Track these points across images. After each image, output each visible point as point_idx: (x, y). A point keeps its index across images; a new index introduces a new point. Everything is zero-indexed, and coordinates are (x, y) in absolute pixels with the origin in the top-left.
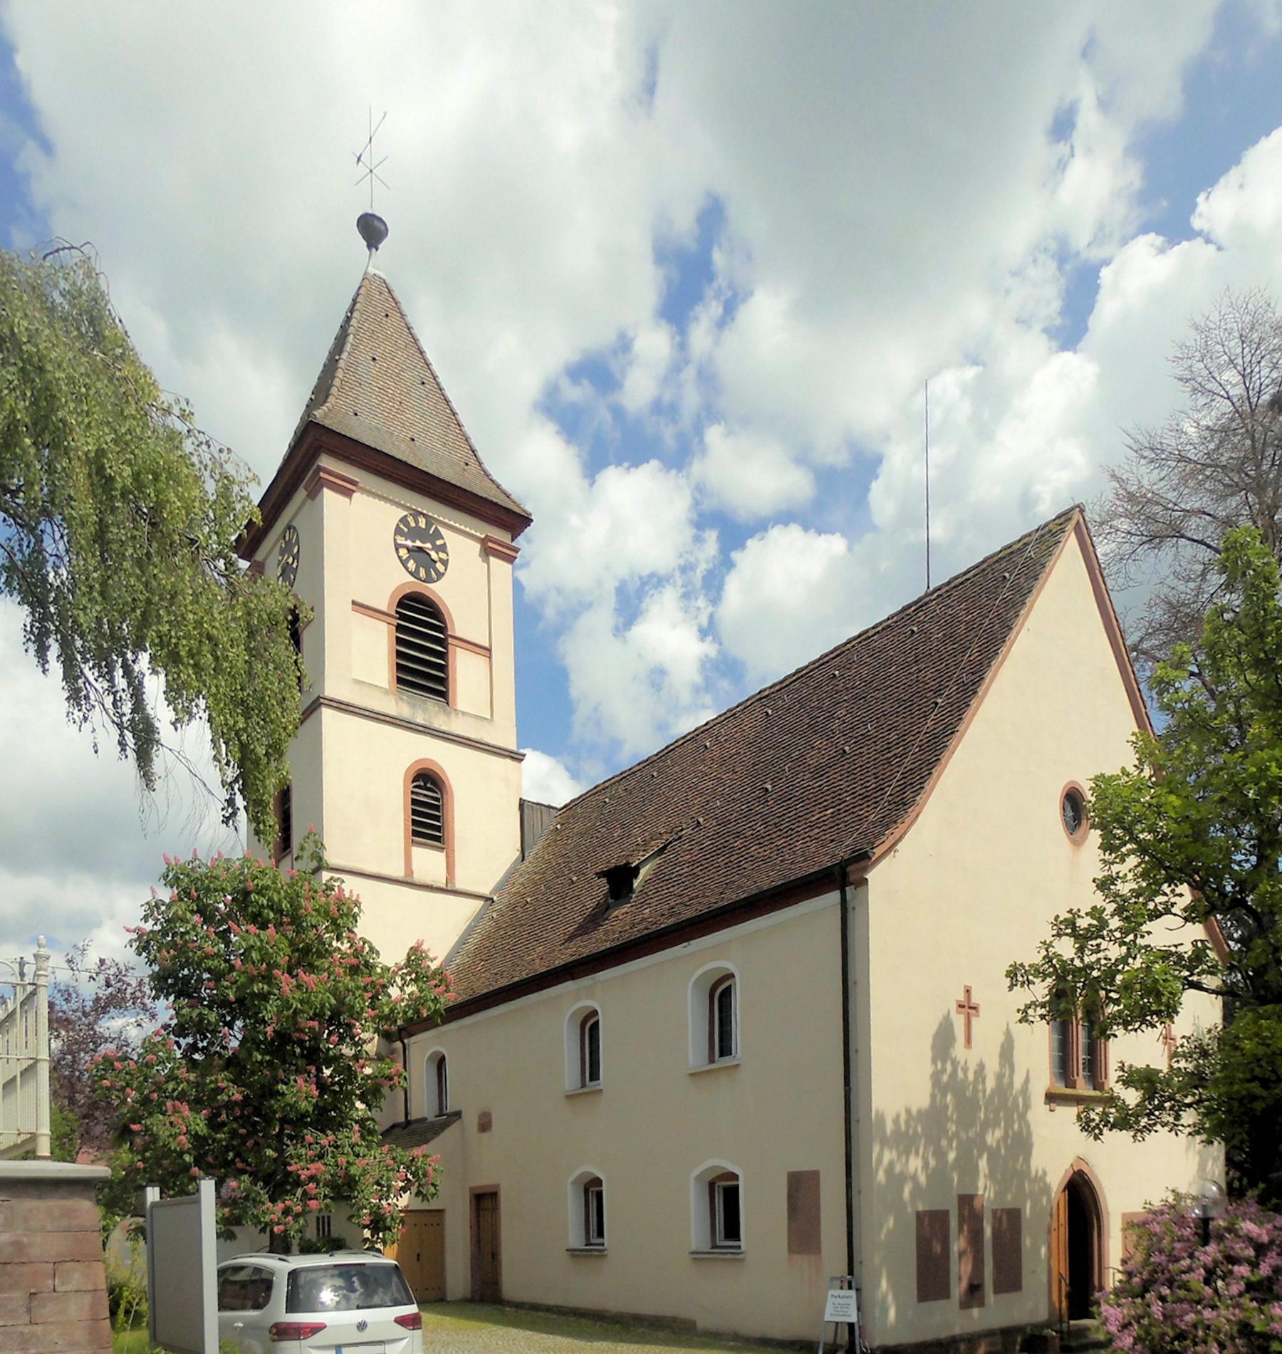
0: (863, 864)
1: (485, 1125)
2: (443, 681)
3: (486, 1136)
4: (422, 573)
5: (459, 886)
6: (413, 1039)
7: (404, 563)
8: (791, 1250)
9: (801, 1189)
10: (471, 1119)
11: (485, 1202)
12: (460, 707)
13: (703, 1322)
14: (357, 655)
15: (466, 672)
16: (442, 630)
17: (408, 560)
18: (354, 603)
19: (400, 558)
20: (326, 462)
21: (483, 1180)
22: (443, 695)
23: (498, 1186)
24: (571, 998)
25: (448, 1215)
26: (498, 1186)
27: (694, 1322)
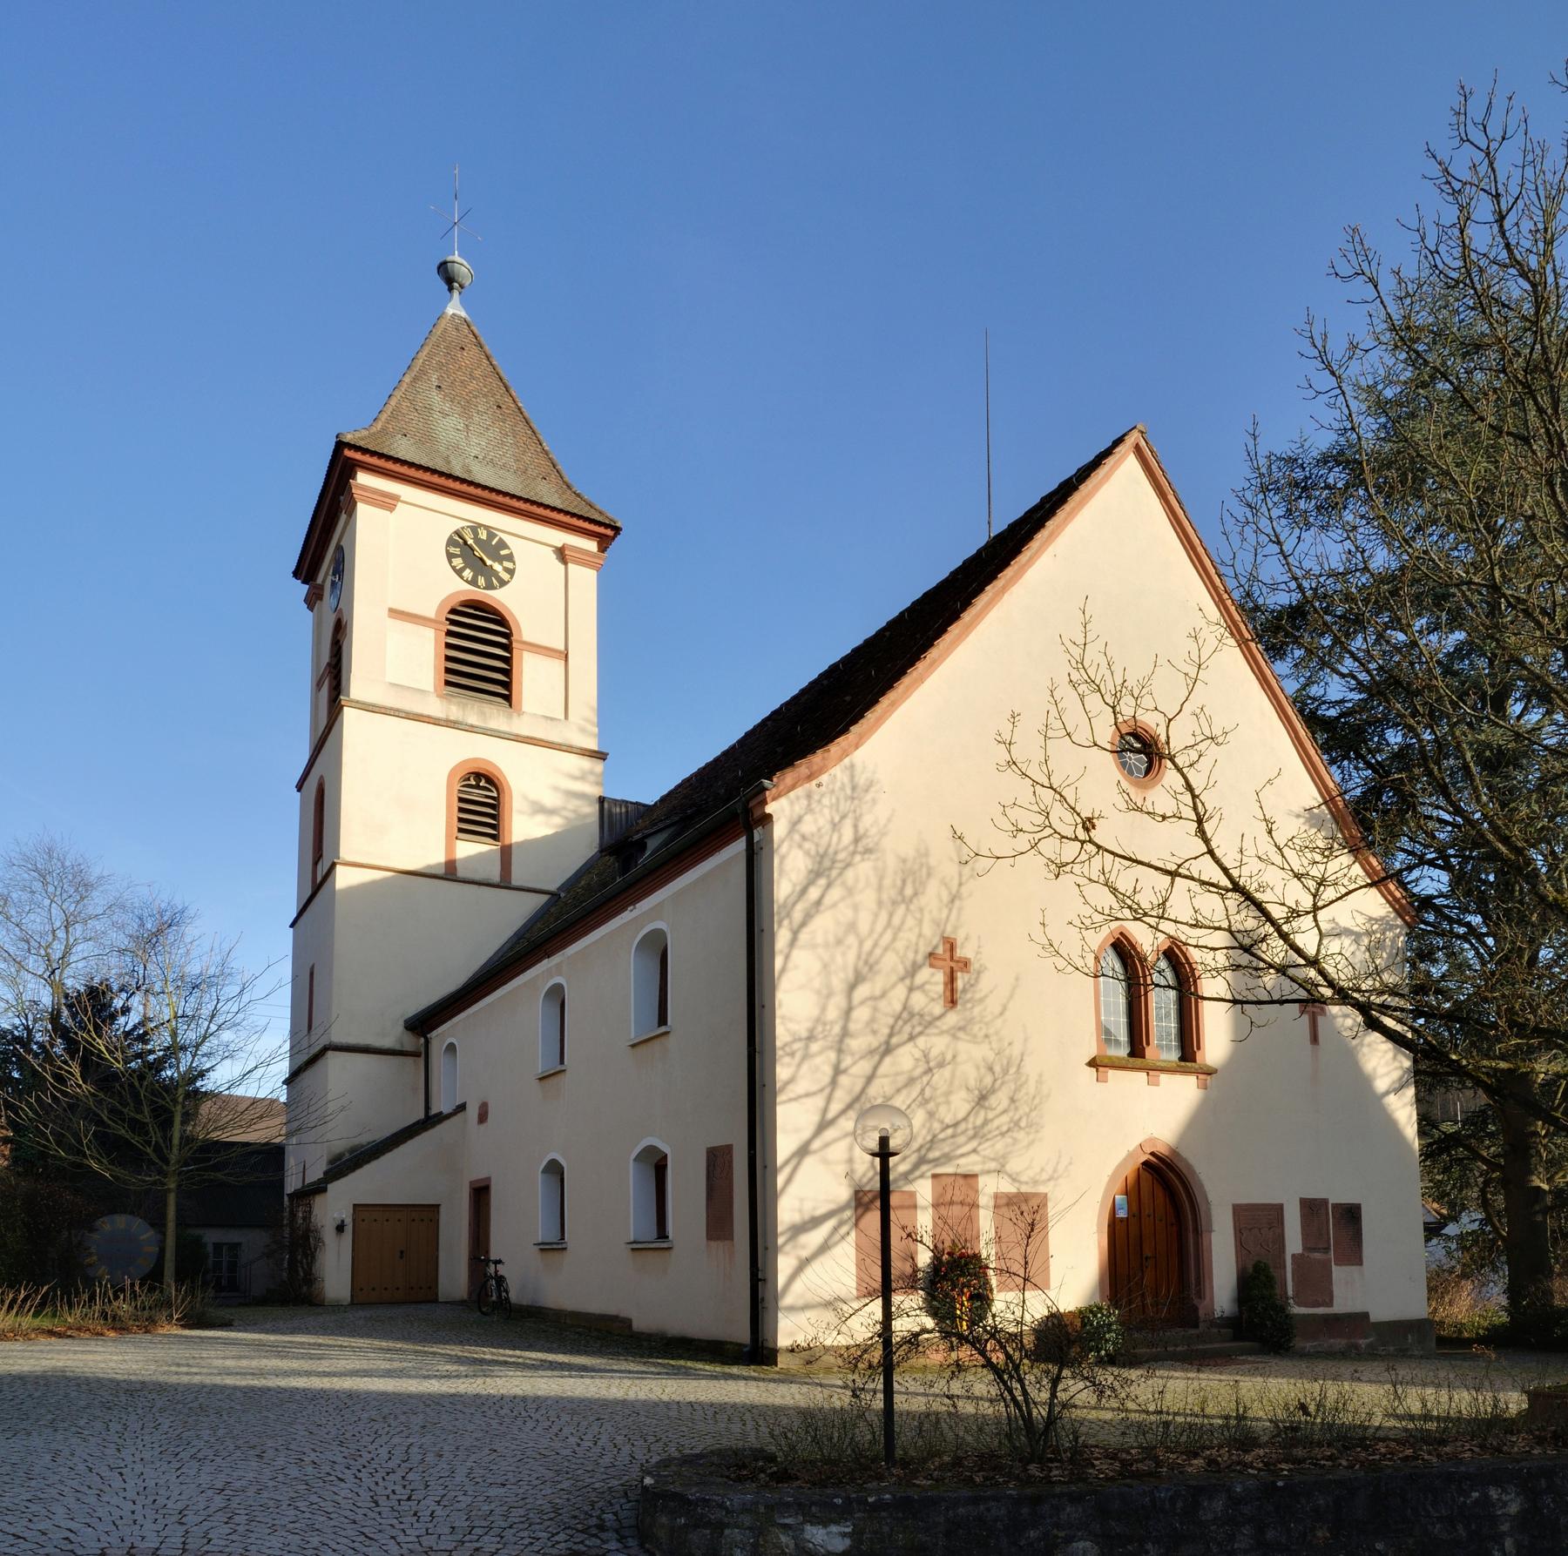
0: (760, 798)
1: (483, 1117)
2: (507, 685)
3: (482, 1127)
4: (481, 581)
5: (515, 883)
6: (434, 1033)
7: (459, 572)
8: (710, 1237)
9: (717, 1160)
10: (472, 1112)
11: (480, 1193)
12: (525, 708)
13: (640, 1323)
14: (395, 653)
15: (532, 674)
16: (508, 636)
17: (462, 570)
18: (391, 610)
19: (454, 568)
20: (363, 478)
21: (479, 1174)
22: (508, 698)
23: (489, 1179)
24: (543, 974)
25: (442, 1209)
26: (489, 1179)
27: (630, 1320)
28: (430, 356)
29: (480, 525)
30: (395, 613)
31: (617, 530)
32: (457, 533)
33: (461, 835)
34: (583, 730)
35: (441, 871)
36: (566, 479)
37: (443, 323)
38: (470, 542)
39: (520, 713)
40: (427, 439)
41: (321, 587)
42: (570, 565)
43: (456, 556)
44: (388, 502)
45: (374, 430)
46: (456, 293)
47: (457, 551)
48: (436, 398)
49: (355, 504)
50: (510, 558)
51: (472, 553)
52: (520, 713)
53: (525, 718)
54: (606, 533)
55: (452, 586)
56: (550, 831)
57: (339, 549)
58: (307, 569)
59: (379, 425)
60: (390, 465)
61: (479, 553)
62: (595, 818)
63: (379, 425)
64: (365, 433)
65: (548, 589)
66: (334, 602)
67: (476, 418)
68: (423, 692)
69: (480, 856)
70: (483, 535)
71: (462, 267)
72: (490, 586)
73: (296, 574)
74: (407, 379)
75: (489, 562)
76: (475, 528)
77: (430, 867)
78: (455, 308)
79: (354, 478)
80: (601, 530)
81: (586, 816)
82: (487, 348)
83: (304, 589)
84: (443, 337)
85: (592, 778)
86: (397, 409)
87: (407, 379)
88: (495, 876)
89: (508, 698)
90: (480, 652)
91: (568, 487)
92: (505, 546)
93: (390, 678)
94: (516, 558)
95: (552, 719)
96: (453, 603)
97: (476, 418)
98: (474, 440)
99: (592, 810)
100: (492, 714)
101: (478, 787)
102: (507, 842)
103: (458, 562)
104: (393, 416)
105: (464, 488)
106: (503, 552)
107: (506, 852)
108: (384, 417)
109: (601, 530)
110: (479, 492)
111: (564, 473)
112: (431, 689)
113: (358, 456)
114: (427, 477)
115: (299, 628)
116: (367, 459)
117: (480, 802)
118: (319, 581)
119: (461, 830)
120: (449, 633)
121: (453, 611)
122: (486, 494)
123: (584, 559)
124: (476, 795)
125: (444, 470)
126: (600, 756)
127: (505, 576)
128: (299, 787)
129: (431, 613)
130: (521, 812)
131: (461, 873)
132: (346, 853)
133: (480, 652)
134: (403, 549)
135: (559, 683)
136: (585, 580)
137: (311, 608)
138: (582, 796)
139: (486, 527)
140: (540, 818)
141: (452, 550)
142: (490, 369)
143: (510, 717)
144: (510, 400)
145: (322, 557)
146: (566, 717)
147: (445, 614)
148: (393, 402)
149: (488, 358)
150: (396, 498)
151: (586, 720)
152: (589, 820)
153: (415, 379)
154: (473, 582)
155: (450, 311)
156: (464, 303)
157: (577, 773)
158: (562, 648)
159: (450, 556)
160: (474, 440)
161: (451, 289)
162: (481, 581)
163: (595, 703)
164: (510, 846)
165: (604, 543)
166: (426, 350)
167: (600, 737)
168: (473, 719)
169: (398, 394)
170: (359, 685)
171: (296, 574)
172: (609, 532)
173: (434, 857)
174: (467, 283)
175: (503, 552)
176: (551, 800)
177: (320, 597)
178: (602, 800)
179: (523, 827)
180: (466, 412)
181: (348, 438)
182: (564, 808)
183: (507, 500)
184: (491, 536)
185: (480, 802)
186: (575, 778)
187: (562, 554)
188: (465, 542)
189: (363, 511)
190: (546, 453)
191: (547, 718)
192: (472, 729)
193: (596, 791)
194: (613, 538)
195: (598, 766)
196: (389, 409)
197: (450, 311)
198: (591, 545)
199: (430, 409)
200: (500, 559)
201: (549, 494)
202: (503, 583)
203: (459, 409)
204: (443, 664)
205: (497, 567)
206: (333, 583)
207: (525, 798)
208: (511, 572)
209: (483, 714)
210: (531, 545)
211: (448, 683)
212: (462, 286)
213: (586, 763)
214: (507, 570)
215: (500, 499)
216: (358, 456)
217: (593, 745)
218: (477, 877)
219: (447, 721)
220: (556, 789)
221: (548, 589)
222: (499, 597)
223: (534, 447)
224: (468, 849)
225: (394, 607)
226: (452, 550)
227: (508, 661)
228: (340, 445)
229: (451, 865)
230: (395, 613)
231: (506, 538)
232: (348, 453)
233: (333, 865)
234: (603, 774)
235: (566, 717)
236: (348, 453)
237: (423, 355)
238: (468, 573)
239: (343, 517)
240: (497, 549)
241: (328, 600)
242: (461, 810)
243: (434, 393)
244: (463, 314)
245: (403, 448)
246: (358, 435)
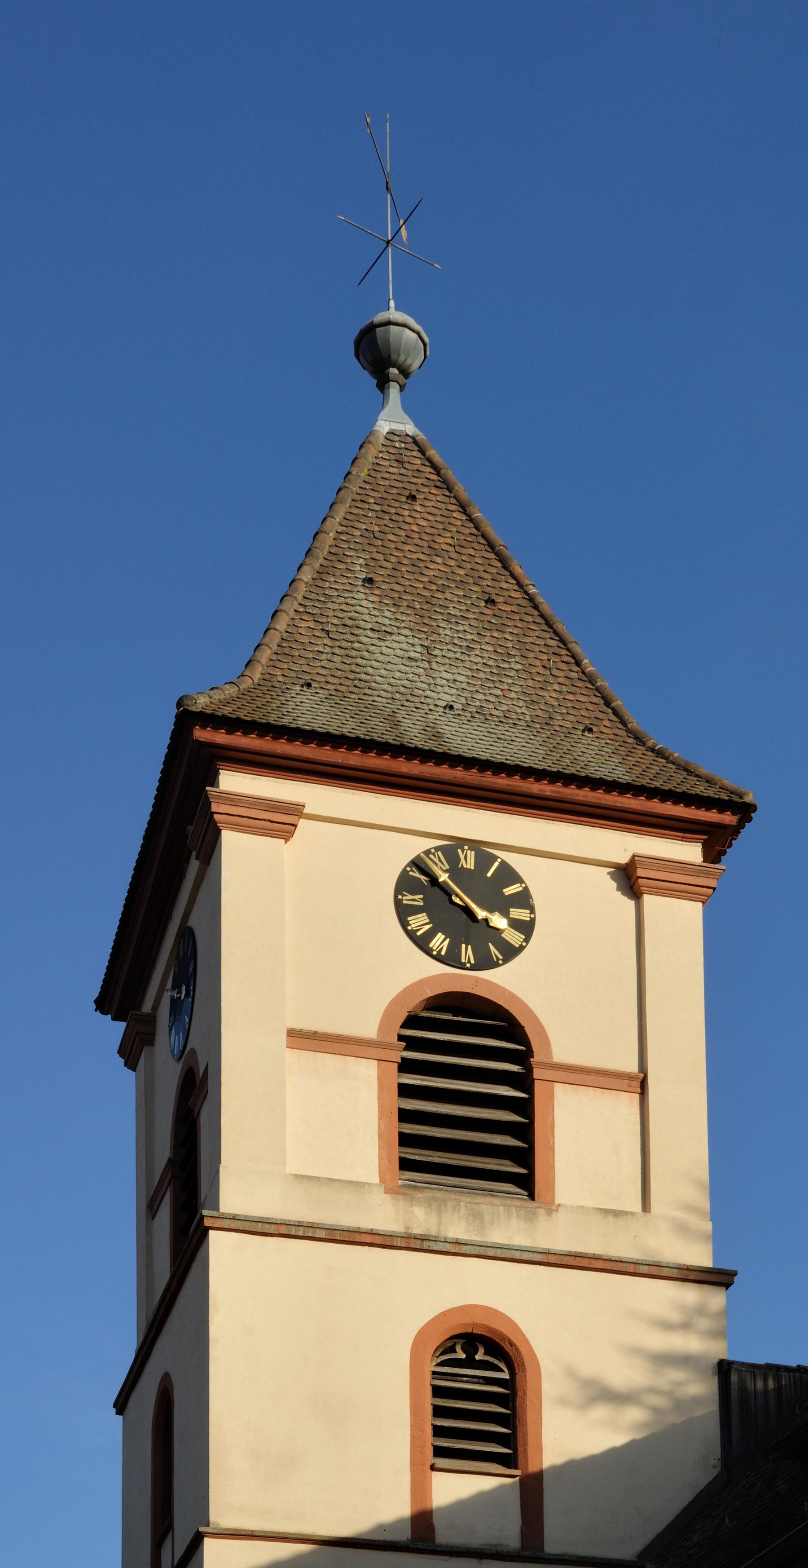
2: (525, 1156)
4: (467, 953)
7: (422, 943)
14: (302, 1120)
15: (579, 1133)
16: (524, 1057)
17: (430, 935)
18: (293, 1034)
19: (411, 935)
20: (232, 781)
22: (526, 1184)
28: (348, 523)
29: (462, 842)
30: (302, 1039)
31: (745, 811)
32: (417, 864)
33: (441, 1462)
34: (682, 1229)
35: (405, 1535)
36: (634, 724)
37: (371, 453)
38: (443, 877)
39: (551, 1208)
40: (351, 685)
41: (151, 1019)
42: (646, 898)
43: (416, 910)
44: (280, 821)
45: (247, 683)
46: (394, 391)
47: (417, 900)
48: (364, 603)
49: (218, 832)
50: (524, 900)
51: (452, 902)
52: (551, 1208)
53: (561, 1217)
54: (718, 820)
55: (412, 970)
56: (619, 1439)
57: (187, 935)
58: (120, 994)
59: (257, 674)
60: (282, 747)
61: (461, 897)
62: (713, 1407)
63: (257, 674)
64: (232, 691)
65: (606, 953)
66: (176, 1040)
67: (446, 632)
68: (356, 1185)
69: (480, 1498)
70: (468, 860)
71: (407, 337)
72: (485, 963)
73: (102, 1004)
74: (307, 575)
75: (481, 914)
76: (452, 848)
77: (382, 1528)
78: (393, 419)
79: (214, 782)
80: (712, 816)
81: (696, 1401)
82: (460, 488)
83: (114, 1030)
84: (371, 480)
85: (704, 1323)
86: (289, 637)
87: (307, 575)
88: (510, 1534)
89: (526, 1184)
90: (468, 1096)
91: (639, 739)
92: (515, 878)
93: (293, 1167)
94: (537, 899)
95: (617, 1214)
96: (412, 1004)
97: (446, 632)
98: (443, 674)
99: (702, 1389)
100: (504, 1220)
101: (470, 1363)
102: (532, 1468)
103: (420, 922)
104: (282, 652)
105: (429, 770)
106: (509, 891)
107: (532, 1488)
108: (265, 656)
109: (712, 816)
110: (458, 774)
111: (628, 715)
112: (376, 1180)
113: (221, 737)
114: (355, 759)
115: (106, 1111)
116: (238, 740)
117: (476, 1388)
118: (147, 1008)
119: (439, 1452)
120: (405, 1066)
121: (411, 1021)
122: (473, 777)
123: (675, 882)
124: (468, 1379)
125: (389, 738)
126: (718, 1278)
127: (514, 937)
128: (121, 1406)
129: (368, 1027)
130: (562, 1402)
131: (443, 1536)
132: (221, 1513)
133: (468, 1096)
134: (313, 910)
135: (631, 1140)
136: (678, 925)
137: (131, 1063)
138: (683, 1361)
139: (475, 845)
140: (601, 1412)
141: (407, 899)
142: (470, 529)
143: (531, 1218)
144: (511, 585)
145: (157, 965)
146: (646, 1205)
147: (396, 1029)
148: (282, 624)
149: (463, 507)
150: (296, 810)
151: (688, 1208)
152: (699, 1412)
153: (322, 574)
154: (451, 959)
155: (383, 426)
156: (408, 408)
157: (675, 1317)
158: (633, 1067)
159: (403, 912)
160: (443, 674)
161: (383, 384)
162: (467, 953)
163: (703, 1173)
164: (539, 1476)
165: (716, 843)
166: (341, 511)
167: (718, 1239)
168: (456, 1228)
169: (290, 606)
170: (238, 1188)
171: (102, 1004)
172: (728, 818)
173: (385, 1504)
174: (415, 362)
175: (509, 891)
176: (624, 1374)
177: (149, 1039)
178: (724, 1368)
179: (566, 1433)
180: (424, 625)
181: (201, 703)
182: (652, 1390)
183: (516, 783)
184: (484, 859)
185: (476, 1388)
186: (666, 1326)
187: (629, 878)
188: (434, 880)
189: (233, 844)
190: (590, 679)
191: (606, 1212)
192: (456, 1249)
193: (718, 1350)
194: (735, 831)
195: (716, 1299)
196: (274, 639)
197: (383, 426)
198: (690, 852)
199: (352, 627)
200: (503, 906)
201: (599, 757)
202: (510, 952)
203: (408, 619)
204: (395, 1127)
205: (498, 921)
206: (175, 1005)
207: (571, 1373)
208: (526, 928)
209: (476, 1216)
210: (563, 866)
211: (406, 1165)
212: (405, 373)
213: (690, 1294)
214: (515, 924)
215: (502, 781)
216: (221, 737)
217: (701, 1256)
218: (475, 1541)
219: (409, 1237)
220: (636, 1352)
221: (606, 953)
222: (506, 982)
223: (563, 670)
224: (454, 1488)
225: (298, 1025)
226: (407, 899)
227: (525, 1107)
228: (187, 719)
229: (422, 1522)
230: (302, 1039)
231: (512, 859)
232: (202, 734)
233: (197, 1540)
234: (727, 1312)
235: (646, 1205)
236: (202, 734)
237: (334, 524)
238: (439, 942)
239: (194, 865)
240: (497, 883)
241: (165, 1040)
242: (438, 1432)
243: (361, 594)
244: (410, 428)
245: (307, 710)
246: (217, 696)
